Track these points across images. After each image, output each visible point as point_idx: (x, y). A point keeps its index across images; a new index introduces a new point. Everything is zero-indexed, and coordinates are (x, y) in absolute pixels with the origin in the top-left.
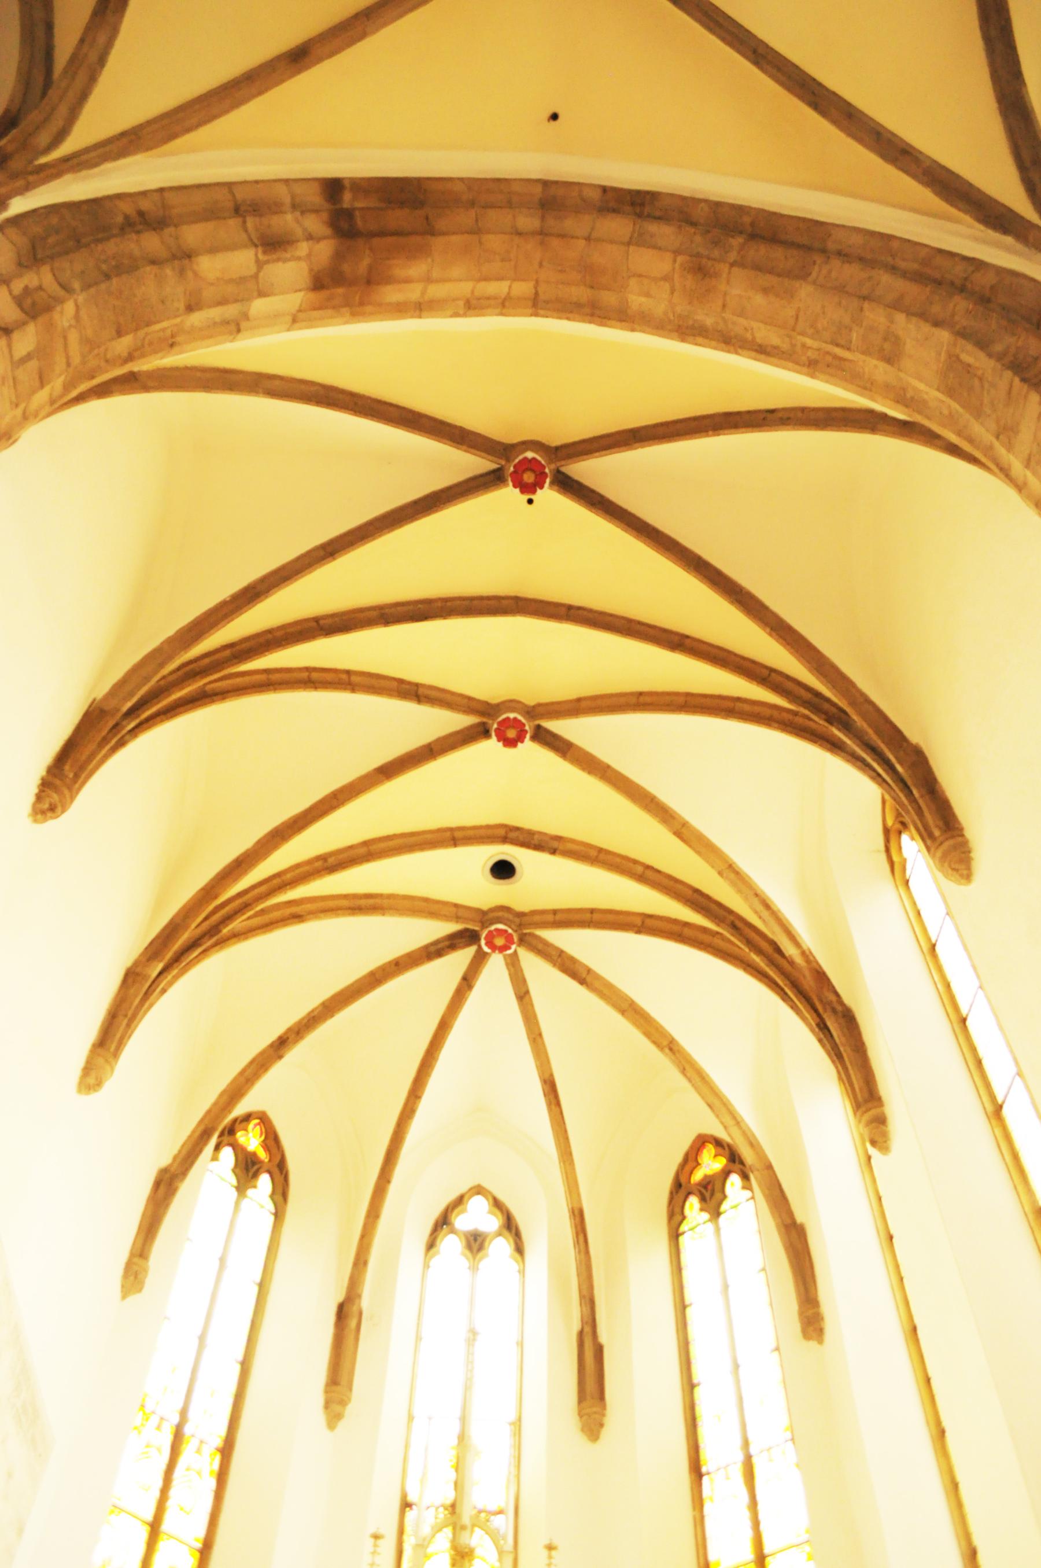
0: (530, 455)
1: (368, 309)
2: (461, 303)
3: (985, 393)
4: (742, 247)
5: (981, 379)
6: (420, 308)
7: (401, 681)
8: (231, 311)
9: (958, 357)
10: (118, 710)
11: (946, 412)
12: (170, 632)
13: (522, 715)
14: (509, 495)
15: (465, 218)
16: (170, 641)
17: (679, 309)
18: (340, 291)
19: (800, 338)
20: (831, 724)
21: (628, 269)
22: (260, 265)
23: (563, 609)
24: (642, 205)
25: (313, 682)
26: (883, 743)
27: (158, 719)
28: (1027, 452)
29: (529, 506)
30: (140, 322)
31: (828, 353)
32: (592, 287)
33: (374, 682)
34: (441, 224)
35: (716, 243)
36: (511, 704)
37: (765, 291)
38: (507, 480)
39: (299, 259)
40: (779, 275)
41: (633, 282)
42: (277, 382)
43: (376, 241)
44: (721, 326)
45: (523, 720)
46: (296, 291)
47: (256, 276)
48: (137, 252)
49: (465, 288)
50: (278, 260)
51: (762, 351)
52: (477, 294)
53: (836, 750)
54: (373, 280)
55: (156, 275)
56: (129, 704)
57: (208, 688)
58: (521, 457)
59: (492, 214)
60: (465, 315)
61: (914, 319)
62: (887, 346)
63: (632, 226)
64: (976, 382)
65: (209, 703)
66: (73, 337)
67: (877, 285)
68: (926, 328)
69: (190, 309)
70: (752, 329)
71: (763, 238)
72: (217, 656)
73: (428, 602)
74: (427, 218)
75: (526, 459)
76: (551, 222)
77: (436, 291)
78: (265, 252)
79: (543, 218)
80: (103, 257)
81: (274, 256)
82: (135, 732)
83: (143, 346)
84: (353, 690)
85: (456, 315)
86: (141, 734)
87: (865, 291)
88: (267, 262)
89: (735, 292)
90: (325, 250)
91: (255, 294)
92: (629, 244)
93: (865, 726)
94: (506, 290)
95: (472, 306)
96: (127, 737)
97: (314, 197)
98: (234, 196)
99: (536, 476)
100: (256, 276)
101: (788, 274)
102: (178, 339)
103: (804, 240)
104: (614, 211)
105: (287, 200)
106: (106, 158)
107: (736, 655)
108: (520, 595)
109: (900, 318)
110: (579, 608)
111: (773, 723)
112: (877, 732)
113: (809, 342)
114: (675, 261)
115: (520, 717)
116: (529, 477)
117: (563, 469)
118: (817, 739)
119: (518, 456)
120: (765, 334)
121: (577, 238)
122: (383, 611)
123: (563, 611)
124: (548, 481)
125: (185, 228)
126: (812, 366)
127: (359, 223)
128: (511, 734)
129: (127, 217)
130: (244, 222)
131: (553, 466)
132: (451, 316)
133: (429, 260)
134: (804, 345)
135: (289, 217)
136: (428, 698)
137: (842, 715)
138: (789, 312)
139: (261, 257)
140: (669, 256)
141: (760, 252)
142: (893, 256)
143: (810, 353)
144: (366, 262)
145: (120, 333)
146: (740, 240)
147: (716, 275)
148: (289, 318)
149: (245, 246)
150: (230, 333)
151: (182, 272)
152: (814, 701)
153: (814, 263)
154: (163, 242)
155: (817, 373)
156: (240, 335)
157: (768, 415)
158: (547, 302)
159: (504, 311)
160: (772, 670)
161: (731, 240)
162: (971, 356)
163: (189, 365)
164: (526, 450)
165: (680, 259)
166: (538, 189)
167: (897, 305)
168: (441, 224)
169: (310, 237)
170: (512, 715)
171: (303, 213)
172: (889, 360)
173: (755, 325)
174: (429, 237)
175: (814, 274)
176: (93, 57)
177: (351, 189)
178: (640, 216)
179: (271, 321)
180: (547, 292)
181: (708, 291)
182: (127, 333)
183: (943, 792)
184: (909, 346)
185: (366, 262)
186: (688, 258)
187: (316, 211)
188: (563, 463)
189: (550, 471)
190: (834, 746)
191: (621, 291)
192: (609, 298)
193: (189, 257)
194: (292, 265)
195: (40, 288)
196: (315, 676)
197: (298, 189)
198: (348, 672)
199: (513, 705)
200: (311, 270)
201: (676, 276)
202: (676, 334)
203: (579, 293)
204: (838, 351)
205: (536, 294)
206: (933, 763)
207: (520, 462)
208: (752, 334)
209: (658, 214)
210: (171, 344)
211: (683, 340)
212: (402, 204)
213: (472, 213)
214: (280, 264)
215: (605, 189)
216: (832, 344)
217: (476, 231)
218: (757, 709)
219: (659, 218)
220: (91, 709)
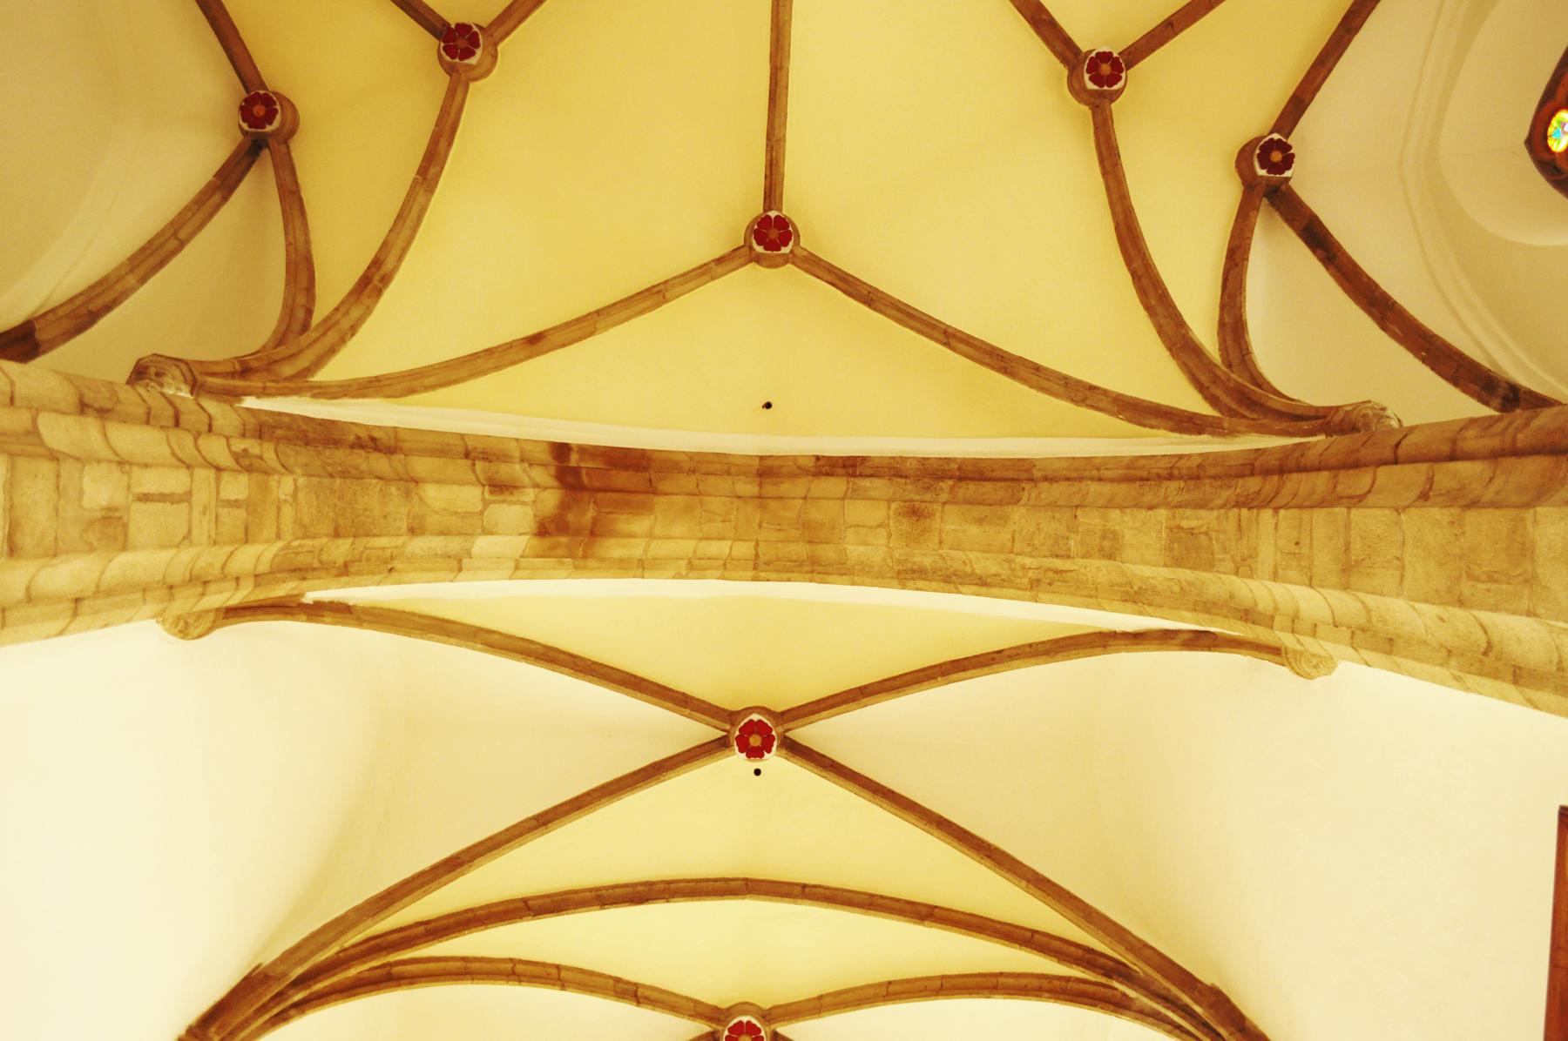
0: (755, 717)
1: (592, 563)
2: (683, 563)
3: (1214, 542)
4: (952, 488)
5: (1206, 534)
6: (642, 567)
7: (618, 980)
8: (454, 544)
9: (1179, 527)
10: (284, 975)
11: (1176, 589)
12: (359, 901)
13: (757, 1019)
14: (736, 760)
15: (689, 482)
16: (356, 910)
17: (897, 554)
18: (564, 540)
19: (1019, 559)
20: (1111, 978)
21: (845, 521)
22: (486, 504)
23: (799, 889)
24: (854, 466)
25: (519, 975)
26: (1174, 985)
27: (333, 997)
28: (1273, 563)
29: (770, 400)
30: (360, 530)
31: (1049, 569)
32: (810, 542)
33: (586, 979)
34: (664, 486)
35: (927, 489)
36: (744, 1007)
37: (980, 521)
38: (732, 746)
39: (524, 503)
40: (990, 505)
41: (851, 535)
42: (496, 637)
43: (600, 495)
44: (941, 564)
45: (758, 1025)
46: (520, 534)
47: (481, 513)
48: (364, 467)
49: (687, 547)
50: (504, 501)
51: (983, 584)
52: (699, 553)
53: (1121, 1010)
54: (596, 532)
55: (381, 490)
56: (299, 971)
57: (396, 970)
58: (746, 720)
59: (712, 480)
60: (686, 577)
61: (1128, 511)
62: (1106, 544)
63: (845, 483)
64: (1203, 538)
65: (395, 987)
66: (288, 512)
67: (1087, 494)
68: (1142, 514)
69: (413, 531)
70: (970, 561)
71: (972, 479)
72: (408, 933)
73: (650, 884)
74: (650, 480)
75: (751, 721)
76: (769, 489)
77: (659, 548)
78: (491, 492)
79: (760, 485)
80: (330, 461)
81: (500, 498)
82: (302, 1006)
83: (360, 561)
84: (563, 987)
85: (678, 576)
86: (310, 1011)
87: (1076, 501)
88: (494, 502)
89: (950, 527)
90: (551, 499)
91: (479, 530)
92: (843, 499)
93: (1150, 971)
94: (727, 551)
95: (694, 567)
96: (292, 1012)
97: (546, 456)
98: (465, 443)
99: (763, 739)
100: (481, 513)
101: (1001, 503)
102: (396, 564)
103: (1010, 474)
104: (828, 474)
105: (517, 454)
106: (345, 395)
107: (993, 921)
108: (749, 877)
109: (1115, 514)
110: (816, 886)
111: (1043, 993)
112: (1166, 976)
113: (1028, 561)
114: (889, 508)
115: (754, 1021)
116: (755, 741)
117: (789, 734)
118: (1097, 1002)
119: (743, 720)
120: (986, 565)
121: (795, 498)
122: (600, 893)
123: (798, 890)
124: (775, 744)
125: (415, 458)
126: (1037, 587)
127: (585, 480)
128: (755, 741)
129: (358, 438)
130: (474, 465)
131: (780, 729)
132: (674, 578)
133: (652, 517)
134: (1023, 568)
135: (517, 467)
136: (649, 1000)
137: (1121, 967)
138: (1006, 536)
139: (487, 496)
140: (883, 505)
141: (970, 489)
142: (1098, 469)
143: (1030, 574)
144: (591, 514)
145: (337, 534)
146: (950, 482)
147: (930, 515)
148: (512, 564)
149: (470, 483)
150: (451, 570)
151: (407, 494)
152: (1086, 957)
153: (1023, 489)
154: (391, 466)
155: (1040, 595)
156: (461, 575)
157: (995, 655)
158: (767, 563)
159: (726, 574)
160: (1034, 932)
161: (941, 484)
162: (1192, 519)
163: (407, 610)
164: (751, 713)
165: (894, 506)
166: (757, 461)
167: (1110, 504)
168: (664, 486)
169: (536, 486)
170: (745, 1019)
171: (530, 465)
172: (1110, 556)
173: (972, 555)
174: (652, 496)
175: (1025, 499)
176: (345, 324)
177: (578, 451)
178: (853, 475)
179: (492, 565)
180: (766, 552)
181: (924, 531)
182: (346, 537)
183: (1255, 1027)
184: (1128, 535)
185: (591, 514)
186: (902, 504)
187: (544, 465)
188: (790, 725)
189: (778, 734)
190: (1119, 1005)
191: (839, 543)
192: (827, 552)
193: (416, 481)
194: (517, 508)
195: (261, 458)
196: (520, 968)
197: (528, 447)
198: (558, 967)
199: (746, 1007)
200: (535, 516)
201: (892, 522)
202: (895, 582)
203: (799, 550)
204: (1059, 564)
205: (757, 555)
206: (1234, 1000)
207: (735, 1025)
208: (971, 566)
209: (869, 471)
210: (387, 567)
211: (904, 587)
212: (626, 468)
213: (693, 478)
214: (506, 505)
215: (818, 458)
216: (1052, 556)
217: (697, 493)
218: (1024, 981)
219: (871, 476)
220: (254, 974)
